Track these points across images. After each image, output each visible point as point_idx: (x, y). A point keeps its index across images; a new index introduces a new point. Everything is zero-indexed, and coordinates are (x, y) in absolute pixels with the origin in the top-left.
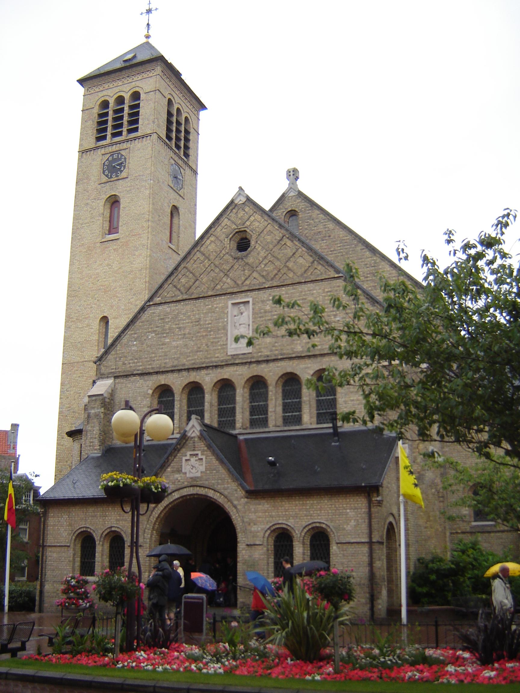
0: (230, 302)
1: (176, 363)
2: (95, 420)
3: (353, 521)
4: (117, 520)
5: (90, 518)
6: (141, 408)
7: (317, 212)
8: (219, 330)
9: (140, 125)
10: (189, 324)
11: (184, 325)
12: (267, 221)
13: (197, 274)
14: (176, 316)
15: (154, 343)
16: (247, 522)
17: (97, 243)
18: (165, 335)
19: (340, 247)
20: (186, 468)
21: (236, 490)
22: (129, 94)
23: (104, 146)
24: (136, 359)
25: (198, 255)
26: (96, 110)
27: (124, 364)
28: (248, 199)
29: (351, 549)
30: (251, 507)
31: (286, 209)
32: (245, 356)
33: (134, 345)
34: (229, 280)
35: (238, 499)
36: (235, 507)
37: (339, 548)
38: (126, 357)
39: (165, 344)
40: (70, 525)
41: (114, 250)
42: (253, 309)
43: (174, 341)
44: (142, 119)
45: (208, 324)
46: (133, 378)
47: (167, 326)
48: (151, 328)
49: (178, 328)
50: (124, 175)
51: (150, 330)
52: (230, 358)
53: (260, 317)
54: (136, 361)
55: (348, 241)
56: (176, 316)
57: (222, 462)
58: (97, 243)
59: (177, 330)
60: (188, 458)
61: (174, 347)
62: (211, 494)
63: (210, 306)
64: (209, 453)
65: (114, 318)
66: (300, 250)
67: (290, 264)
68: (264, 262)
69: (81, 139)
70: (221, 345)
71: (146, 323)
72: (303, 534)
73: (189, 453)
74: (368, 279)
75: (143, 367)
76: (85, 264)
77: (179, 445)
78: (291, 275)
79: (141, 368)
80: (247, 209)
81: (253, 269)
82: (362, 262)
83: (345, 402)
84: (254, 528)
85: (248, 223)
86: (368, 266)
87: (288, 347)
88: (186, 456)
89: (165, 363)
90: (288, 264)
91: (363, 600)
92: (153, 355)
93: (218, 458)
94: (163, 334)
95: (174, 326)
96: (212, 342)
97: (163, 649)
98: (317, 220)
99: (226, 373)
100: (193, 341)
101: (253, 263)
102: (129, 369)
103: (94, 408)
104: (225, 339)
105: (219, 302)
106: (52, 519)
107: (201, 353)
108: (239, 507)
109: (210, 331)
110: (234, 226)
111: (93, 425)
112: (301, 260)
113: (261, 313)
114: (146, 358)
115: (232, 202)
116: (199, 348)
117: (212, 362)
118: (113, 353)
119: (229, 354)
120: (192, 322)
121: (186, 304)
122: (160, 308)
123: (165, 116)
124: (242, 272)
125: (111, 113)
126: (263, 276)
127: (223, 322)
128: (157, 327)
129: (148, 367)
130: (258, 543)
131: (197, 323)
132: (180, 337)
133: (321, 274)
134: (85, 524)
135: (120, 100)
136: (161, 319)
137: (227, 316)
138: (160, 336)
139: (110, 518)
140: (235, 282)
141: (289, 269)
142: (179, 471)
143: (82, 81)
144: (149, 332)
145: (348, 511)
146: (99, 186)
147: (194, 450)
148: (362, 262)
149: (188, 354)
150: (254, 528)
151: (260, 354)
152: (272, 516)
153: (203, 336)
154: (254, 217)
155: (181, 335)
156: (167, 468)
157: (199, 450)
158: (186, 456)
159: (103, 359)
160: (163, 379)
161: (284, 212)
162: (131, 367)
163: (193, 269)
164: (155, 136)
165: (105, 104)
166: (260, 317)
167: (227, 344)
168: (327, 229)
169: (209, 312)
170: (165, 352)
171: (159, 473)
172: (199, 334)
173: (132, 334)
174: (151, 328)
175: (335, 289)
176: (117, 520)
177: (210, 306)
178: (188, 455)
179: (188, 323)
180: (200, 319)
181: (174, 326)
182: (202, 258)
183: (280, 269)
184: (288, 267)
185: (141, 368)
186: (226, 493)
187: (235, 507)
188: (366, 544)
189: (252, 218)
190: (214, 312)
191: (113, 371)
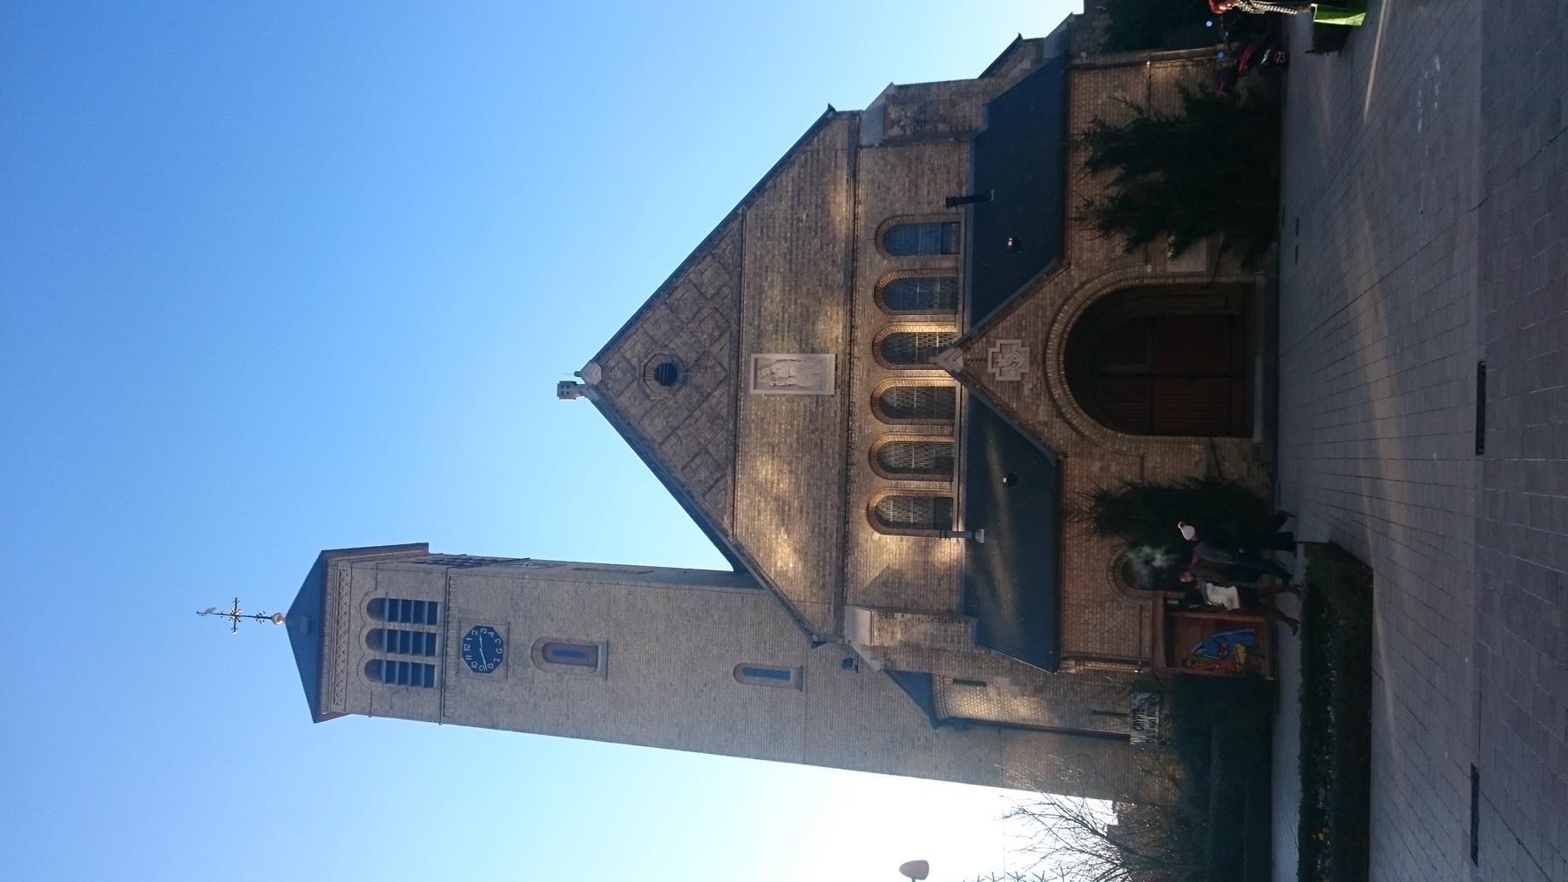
0: (752, 391)
1: (835, 488)
20: (1012, 375)
22: (369, 620)
23: (443, 672)
25: (666, 447)
26: (378, 687)
34: (716, 394)
36: (1082, 285)
40: (1101, 604)
50: (501, 630)
57: (1010, 309)
60: (997, 371)
62: (1057, 327)
64: (992, 333)
67: (711, 291)
69: (420, 718)
73: (990, 370)
78: (726, 290)
80: (612, 363)
81: (705, 353)
83: (929, 203)
85: (634, 361)
93: (1001, 317)
110: (634, 385)
112: (708, 274)
125: (391, 657)
135: (375, 638)
141: (717, 293)
142: (1017, 386)
146: (511, 681)
147: (986, 360)
165: (373, 669)
182: (673, 440)
186: (1060, 302)
187: (1082, 285)
189: (628, 355)
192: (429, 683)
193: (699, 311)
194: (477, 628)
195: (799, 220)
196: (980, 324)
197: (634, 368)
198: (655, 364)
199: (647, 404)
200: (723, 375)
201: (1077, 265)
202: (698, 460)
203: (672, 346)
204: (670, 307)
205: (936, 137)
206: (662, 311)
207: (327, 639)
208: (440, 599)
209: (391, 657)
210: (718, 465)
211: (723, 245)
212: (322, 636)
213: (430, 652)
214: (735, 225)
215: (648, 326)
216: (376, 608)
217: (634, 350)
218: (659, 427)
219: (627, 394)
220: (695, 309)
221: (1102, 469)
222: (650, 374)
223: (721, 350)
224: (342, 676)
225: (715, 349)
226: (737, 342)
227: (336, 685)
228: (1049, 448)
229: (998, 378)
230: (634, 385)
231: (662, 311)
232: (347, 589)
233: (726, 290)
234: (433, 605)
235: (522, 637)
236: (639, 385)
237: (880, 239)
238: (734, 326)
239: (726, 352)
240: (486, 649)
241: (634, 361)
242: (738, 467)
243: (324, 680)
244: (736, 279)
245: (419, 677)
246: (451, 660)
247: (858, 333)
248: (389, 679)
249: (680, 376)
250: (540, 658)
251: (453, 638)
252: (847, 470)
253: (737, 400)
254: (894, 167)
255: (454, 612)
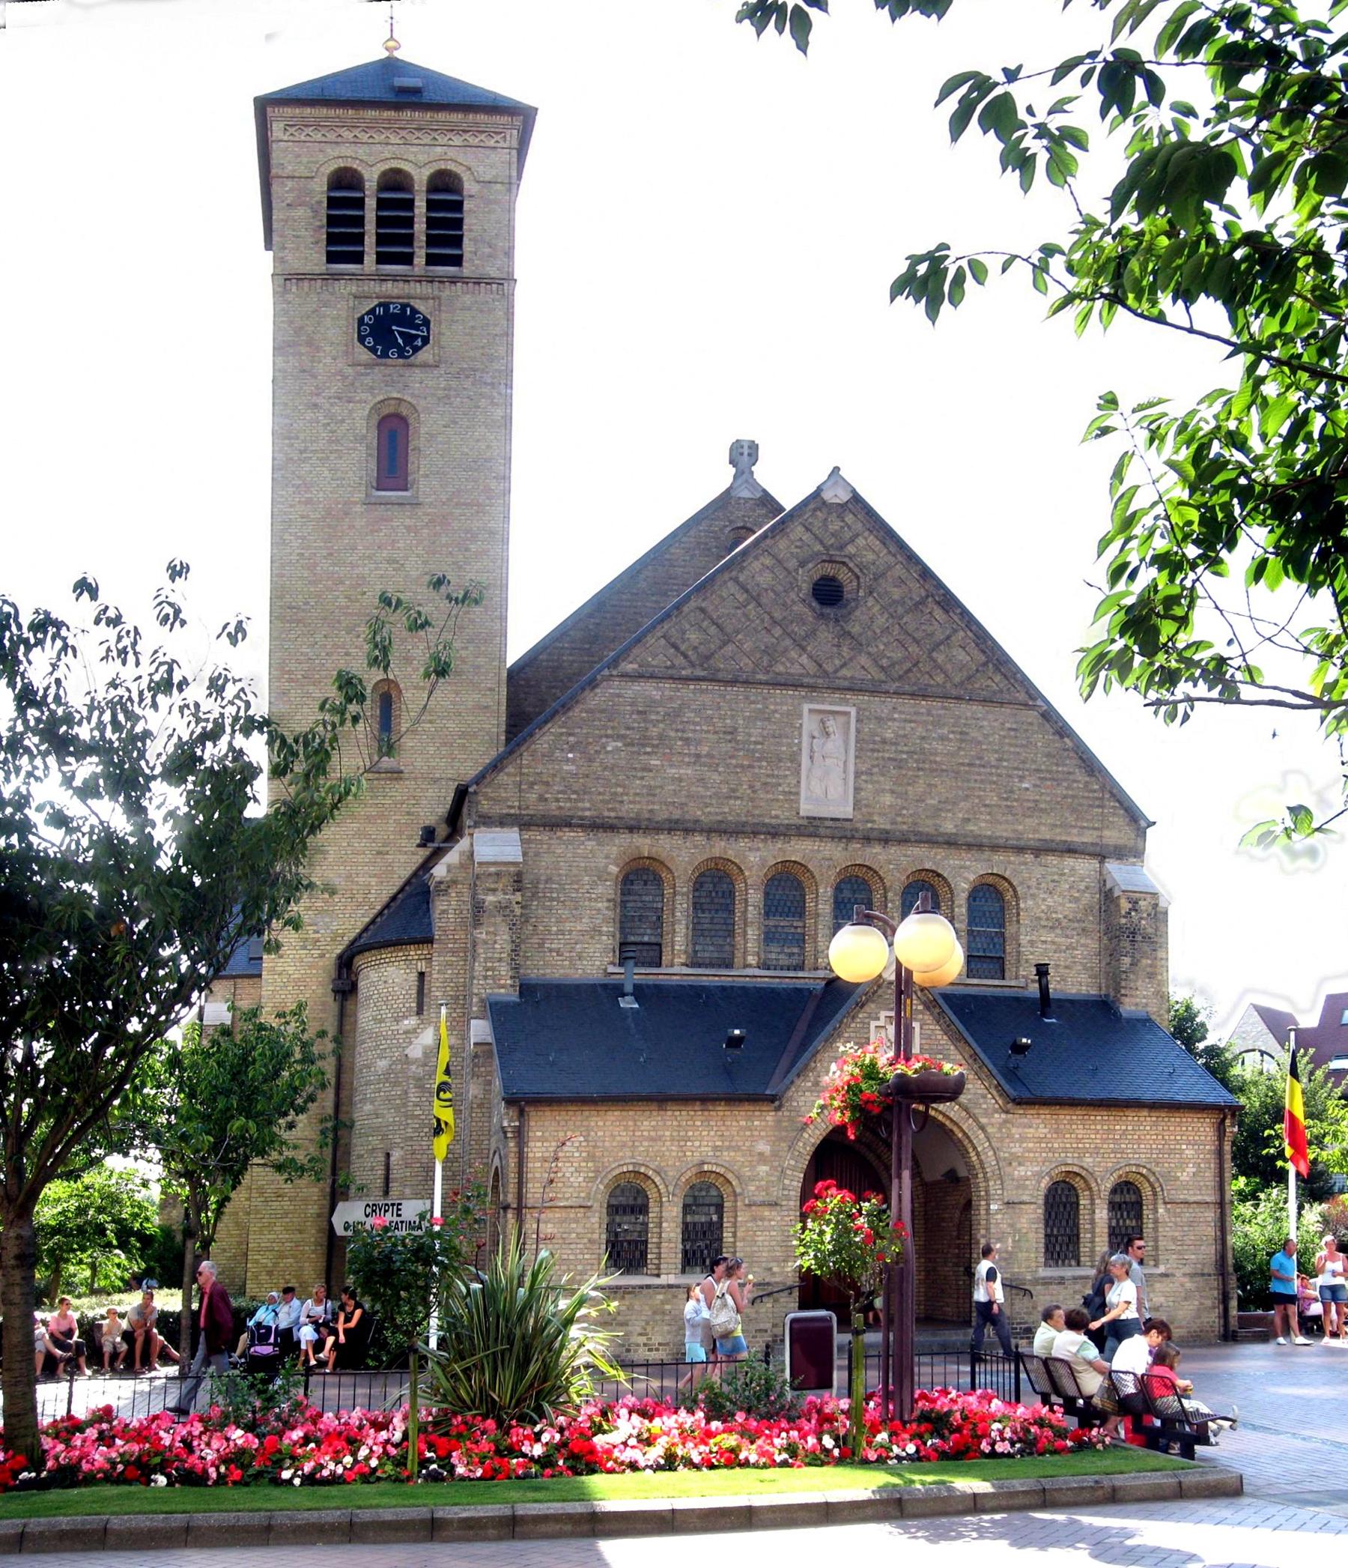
0: (806, 707)
1: (677, 814)
2: (499, 919)
4: (715, 1148)
5: (646, 1144)
6: (590, 899)
8: (780, 760)
10: (710, 736)
11: (697, 736)
12: (894, 555)
13: (729, 629)
14: (677, 713)
15: (623, 763)
16: (1005, 1159)
17: (356, 503)
18: (649, 750)
21: (984, 1097)
23: (352, 276)
24: (575, 792)
25: (732, 587)
27: (542, 799)
28: (856, 498)
29: (1188, 1214)
30: (1014, 1130)
32: (838, 824)
33: (568, 760)
34: (804, 659)
35: (986, 1114)
36: (982, 1128)
37: (1168, 1211)
38: (547, 784)
39: (651, 771)
40: (591, 1157)
41: (408, 528)
42: (858, 731)
43: (671, 766)
44: (475, 240)
45: (756, 743)
46: (568, 834)
47: (654, 732)
48: (613, 728)
49: (681, 739)
50: (425, 355)
51: (609, 732)
52: (805, 822)
53: (873, 750)
54: (574, 796)
56: (677, 713)
58: (356, 503)
59: (680, 743)
60: (881, 1023)
61: (673, 779)
63: (760, 706)
65: (415, 688)
66: (961, 634)
67: (940, 658)
70: (784, 793)
71: (598, 715)
75: (595, 813)
79: (587, 813)
80: (849, 518)
81: (858, 646)
83: (1032, 943)
84: (1021, 1171)
85: (851, 549)
87: (929, 822)
88: (878, 1019)
89: (651, 811)
90: (934, 654)
91: (1209, 1303)
92: (620, 790)
94: (644, 746)
95: (672, 734)
96: (765, 784)
99: (798, 850)
100: (720, 774)
102: (557, 813)
103: (494, 890)
104: (794, 782)
105: (781, 700)
106: (539, 1144)
107: (738, 802)
108: (990, 1130)
109: (760, 760)
110: (818, 547)
111: (492, 929)
112: (961, 656)
113: (874, 742)
114: (600, 794)
115: (817, 494)
116: (734, 791)
117: (764, 825)
118: (510, 769)
119: (802, 814)
120: (716, 733)
121: (702, 691)
122: (637, 687)
124: (835, 649)
125: (371, 203)
126: (882, 667)
127: (789, 745)
128: (628, 728)
129: (606, 814)
130: (1026, 1198)
131: (729, 737)
132: (687, 760)
133: (1001, 691)
134: (633, 1157)
136: (639, 713)
137: (800, 735)
138: (635, 749)
139: (697, 1144)
140: (820, 666)
141: (937, 666)
144: (607, 736)
146: (350, 370)
149: (708, 801)
150: (1021, 1171)
151: (869, 825)
152: (1051, 1150)
153: (742, 766)
155: (689, 755)
158: (878, 1019)
159: (486, 781)
160: (644, 844)
162: (560, 808)
163: (719, 617)
165: (345, 181)
166: (873, 750)
167: (798, 794)
169: (756, 718)
170: (650, 787)
172: (734, 762)
173: (562, 734)
174: (613, 728)
176: (715, 1148)
177: (760, 706)
178: (882, 1018)
179: (708, 732)
180: (736, 729)
181: (672, 734)
182: (742, 597)
184: (935, 661)
185: (586, 809)
187: (982, 1128)
189: (860, 541)
190: (768, 719)
191: (512, 811)
192: (332, 258)
193: (917, 642)
194: (426, 322)
195: (1022, 778)
196: (941, 1001)
197: (841, 548)
198: (843, 576)
199: (792, 564)
200: (830, 668)
201: (1005, 1121)
202: (713, 630)
203: (871, 602)
204: (922, 602)
205: (1112, 954)
206: (917, 591)
207: (391, 114)
208: (467, 269)
209: (371, 203)
210: (708, 658)
211: (998, 678)
212: (397, 107)
213: (382, 258)
214: (1022, 696)
215: (899, 571)
216: (445, 184)
217: (866, 549)
218: (759, 579)
219: (806, 537)
220: (918, 635)
221: (761, 1154)
222: (829, 570)
223: (861, 667)
224: (331, 136)
225: (863, 660)
226: (874, 690)
227: (318, 127)
228: (788, 1088)
229: (873, 1024)
230: (818, 547)
231: (917, 591)
232: (475, 141)
233: (940, 679)
234: (457, 261)
235: (415, 384)
236: (818, 554)
237: (991, 880)
238: (893, 686)
239: (860, 674)
240: (393, 332)
241: (851, 549)
242: (704, 685)
243: (324, 111)
244: (954, 692)
245: (342, 242)
246: (375, 287)
247: (877, 849)
248: (332, 203)
249: (827, 610)
250: (386, 411)
251: (410, 286)
252: (702, 831)
253: (796, 686)
254: (1077, 900)
255: (447, 291)
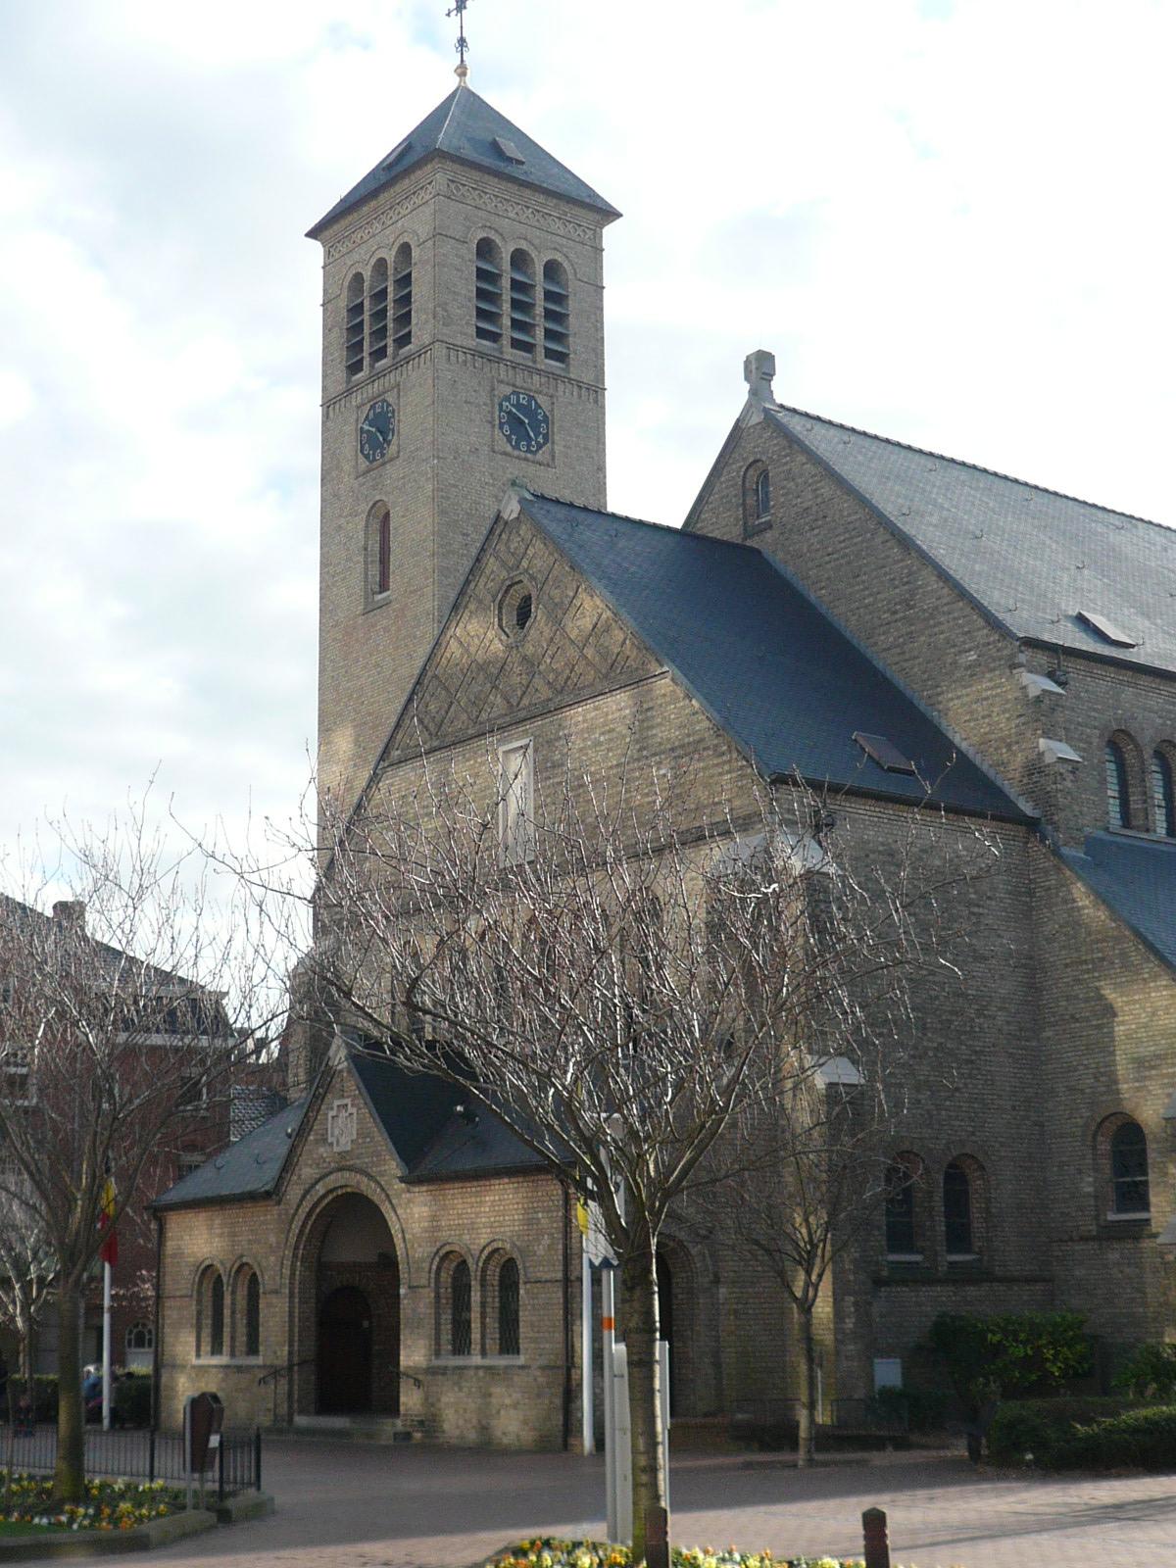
3: (546, 1237)
7: (802, 458)
9: (414, 329)
19: (844, 541)
31: (744, 459)
50: (392, 449)
55: (857, 524)
68: (549, 652)
72: (481, 1264)
73: (337, 1103)
74: (898, 616)
76: (342, 667)
77: (322, 1087)
82: (885, 574)
86: (896, 582)
97: (663, 1504)
98: (800, 481)
101: (533, 655)
123: (469, 286)
143: (313, 234)
145: (540, 1215)
148: (885, 574)
154: (534, 546)
156: (309, 1134)
157: (348, 1097)
161: (741, 467)
164: (439, 350)
168: (819, 500)
171: (298, 1145)
175: (659, 702)
183: (574, 666)
188: (558, 1284)
